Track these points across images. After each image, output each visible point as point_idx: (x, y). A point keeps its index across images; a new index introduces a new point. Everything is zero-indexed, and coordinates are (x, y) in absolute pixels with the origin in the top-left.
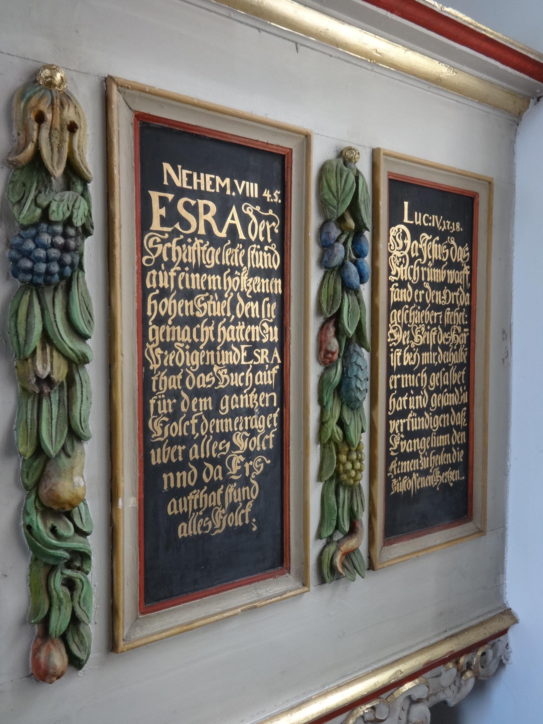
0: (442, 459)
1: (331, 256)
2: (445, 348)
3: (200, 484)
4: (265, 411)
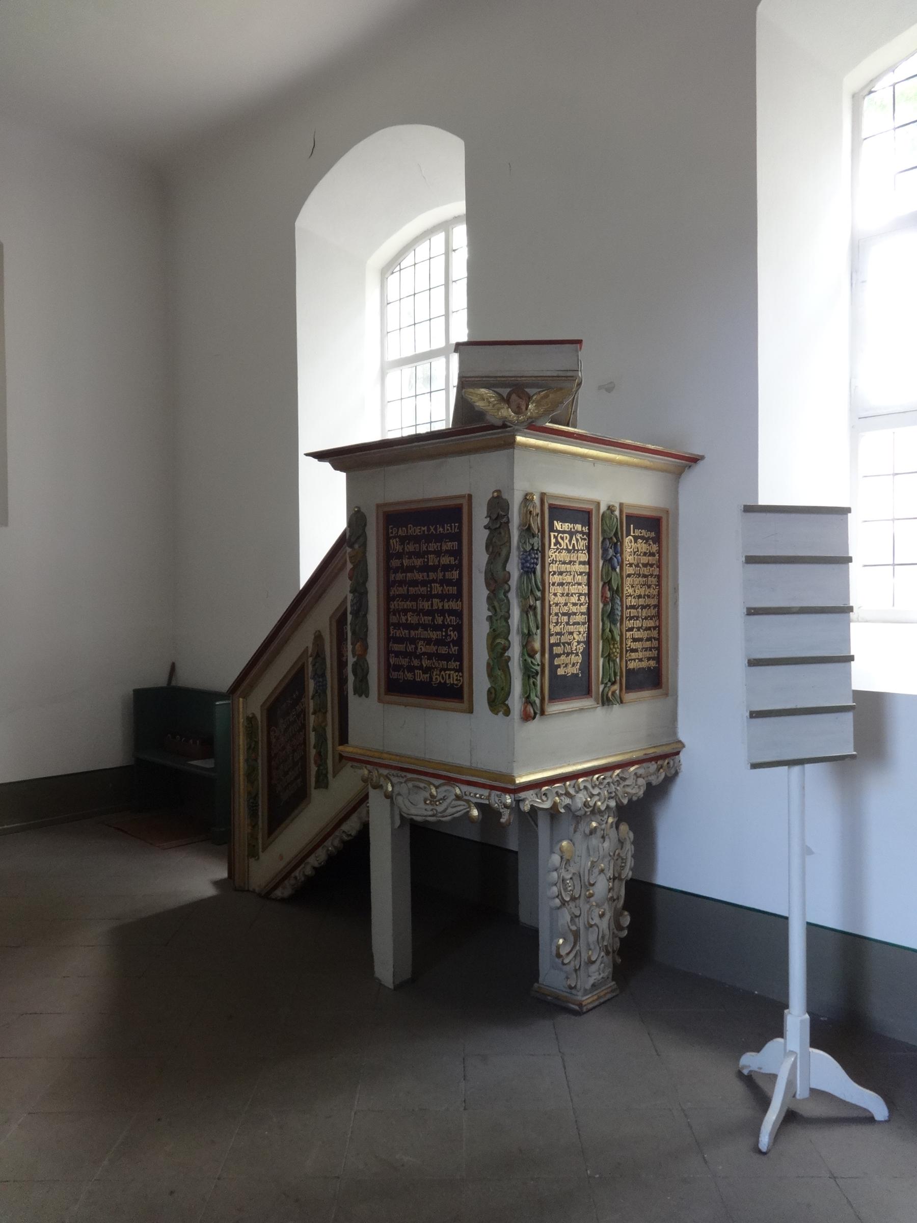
0: (648, 654)
1: (608, 554)
2: (649, 596)
3: (564, 653)
4: (584, 624)
